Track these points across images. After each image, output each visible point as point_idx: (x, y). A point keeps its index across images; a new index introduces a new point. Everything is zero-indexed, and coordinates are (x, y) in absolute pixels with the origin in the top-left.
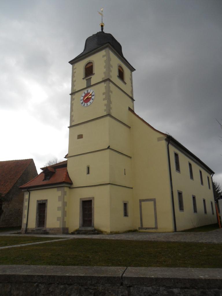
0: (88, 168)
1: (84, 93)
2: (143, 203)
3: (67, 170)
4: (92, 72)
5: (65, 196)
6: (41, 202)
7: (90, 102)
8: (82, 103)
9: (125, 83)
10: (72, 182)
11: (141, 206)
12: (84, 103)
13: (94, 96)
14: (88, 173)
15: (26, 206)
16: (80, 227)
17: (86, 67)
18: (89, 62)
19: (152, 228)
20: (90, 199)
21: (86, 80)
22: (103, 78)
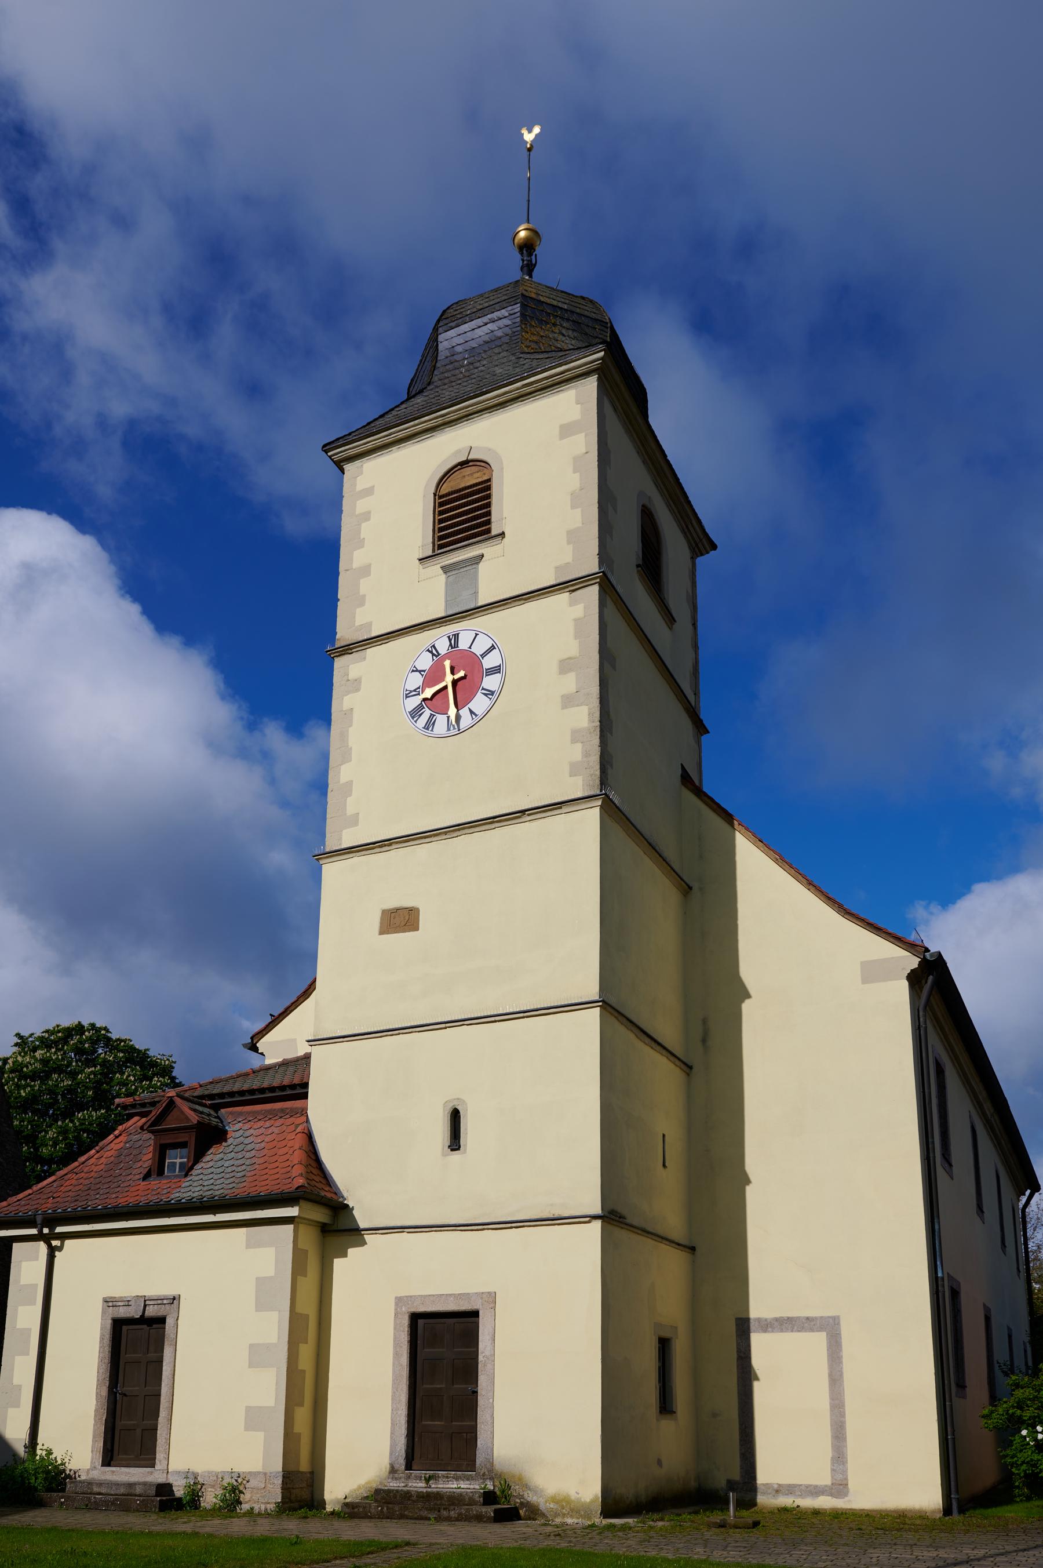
0: (455, 1116)
1: (433, 650)
3: (308, 1121)
4: (489, 522)
5: (300, 1279)
6: (134, 1312)
7: (471, 712)
8: (416, 713)
11: (839, 1457)
12: (427, 712)
16: (393, 1470)
19: (816, 1491)
21: (446, 569)
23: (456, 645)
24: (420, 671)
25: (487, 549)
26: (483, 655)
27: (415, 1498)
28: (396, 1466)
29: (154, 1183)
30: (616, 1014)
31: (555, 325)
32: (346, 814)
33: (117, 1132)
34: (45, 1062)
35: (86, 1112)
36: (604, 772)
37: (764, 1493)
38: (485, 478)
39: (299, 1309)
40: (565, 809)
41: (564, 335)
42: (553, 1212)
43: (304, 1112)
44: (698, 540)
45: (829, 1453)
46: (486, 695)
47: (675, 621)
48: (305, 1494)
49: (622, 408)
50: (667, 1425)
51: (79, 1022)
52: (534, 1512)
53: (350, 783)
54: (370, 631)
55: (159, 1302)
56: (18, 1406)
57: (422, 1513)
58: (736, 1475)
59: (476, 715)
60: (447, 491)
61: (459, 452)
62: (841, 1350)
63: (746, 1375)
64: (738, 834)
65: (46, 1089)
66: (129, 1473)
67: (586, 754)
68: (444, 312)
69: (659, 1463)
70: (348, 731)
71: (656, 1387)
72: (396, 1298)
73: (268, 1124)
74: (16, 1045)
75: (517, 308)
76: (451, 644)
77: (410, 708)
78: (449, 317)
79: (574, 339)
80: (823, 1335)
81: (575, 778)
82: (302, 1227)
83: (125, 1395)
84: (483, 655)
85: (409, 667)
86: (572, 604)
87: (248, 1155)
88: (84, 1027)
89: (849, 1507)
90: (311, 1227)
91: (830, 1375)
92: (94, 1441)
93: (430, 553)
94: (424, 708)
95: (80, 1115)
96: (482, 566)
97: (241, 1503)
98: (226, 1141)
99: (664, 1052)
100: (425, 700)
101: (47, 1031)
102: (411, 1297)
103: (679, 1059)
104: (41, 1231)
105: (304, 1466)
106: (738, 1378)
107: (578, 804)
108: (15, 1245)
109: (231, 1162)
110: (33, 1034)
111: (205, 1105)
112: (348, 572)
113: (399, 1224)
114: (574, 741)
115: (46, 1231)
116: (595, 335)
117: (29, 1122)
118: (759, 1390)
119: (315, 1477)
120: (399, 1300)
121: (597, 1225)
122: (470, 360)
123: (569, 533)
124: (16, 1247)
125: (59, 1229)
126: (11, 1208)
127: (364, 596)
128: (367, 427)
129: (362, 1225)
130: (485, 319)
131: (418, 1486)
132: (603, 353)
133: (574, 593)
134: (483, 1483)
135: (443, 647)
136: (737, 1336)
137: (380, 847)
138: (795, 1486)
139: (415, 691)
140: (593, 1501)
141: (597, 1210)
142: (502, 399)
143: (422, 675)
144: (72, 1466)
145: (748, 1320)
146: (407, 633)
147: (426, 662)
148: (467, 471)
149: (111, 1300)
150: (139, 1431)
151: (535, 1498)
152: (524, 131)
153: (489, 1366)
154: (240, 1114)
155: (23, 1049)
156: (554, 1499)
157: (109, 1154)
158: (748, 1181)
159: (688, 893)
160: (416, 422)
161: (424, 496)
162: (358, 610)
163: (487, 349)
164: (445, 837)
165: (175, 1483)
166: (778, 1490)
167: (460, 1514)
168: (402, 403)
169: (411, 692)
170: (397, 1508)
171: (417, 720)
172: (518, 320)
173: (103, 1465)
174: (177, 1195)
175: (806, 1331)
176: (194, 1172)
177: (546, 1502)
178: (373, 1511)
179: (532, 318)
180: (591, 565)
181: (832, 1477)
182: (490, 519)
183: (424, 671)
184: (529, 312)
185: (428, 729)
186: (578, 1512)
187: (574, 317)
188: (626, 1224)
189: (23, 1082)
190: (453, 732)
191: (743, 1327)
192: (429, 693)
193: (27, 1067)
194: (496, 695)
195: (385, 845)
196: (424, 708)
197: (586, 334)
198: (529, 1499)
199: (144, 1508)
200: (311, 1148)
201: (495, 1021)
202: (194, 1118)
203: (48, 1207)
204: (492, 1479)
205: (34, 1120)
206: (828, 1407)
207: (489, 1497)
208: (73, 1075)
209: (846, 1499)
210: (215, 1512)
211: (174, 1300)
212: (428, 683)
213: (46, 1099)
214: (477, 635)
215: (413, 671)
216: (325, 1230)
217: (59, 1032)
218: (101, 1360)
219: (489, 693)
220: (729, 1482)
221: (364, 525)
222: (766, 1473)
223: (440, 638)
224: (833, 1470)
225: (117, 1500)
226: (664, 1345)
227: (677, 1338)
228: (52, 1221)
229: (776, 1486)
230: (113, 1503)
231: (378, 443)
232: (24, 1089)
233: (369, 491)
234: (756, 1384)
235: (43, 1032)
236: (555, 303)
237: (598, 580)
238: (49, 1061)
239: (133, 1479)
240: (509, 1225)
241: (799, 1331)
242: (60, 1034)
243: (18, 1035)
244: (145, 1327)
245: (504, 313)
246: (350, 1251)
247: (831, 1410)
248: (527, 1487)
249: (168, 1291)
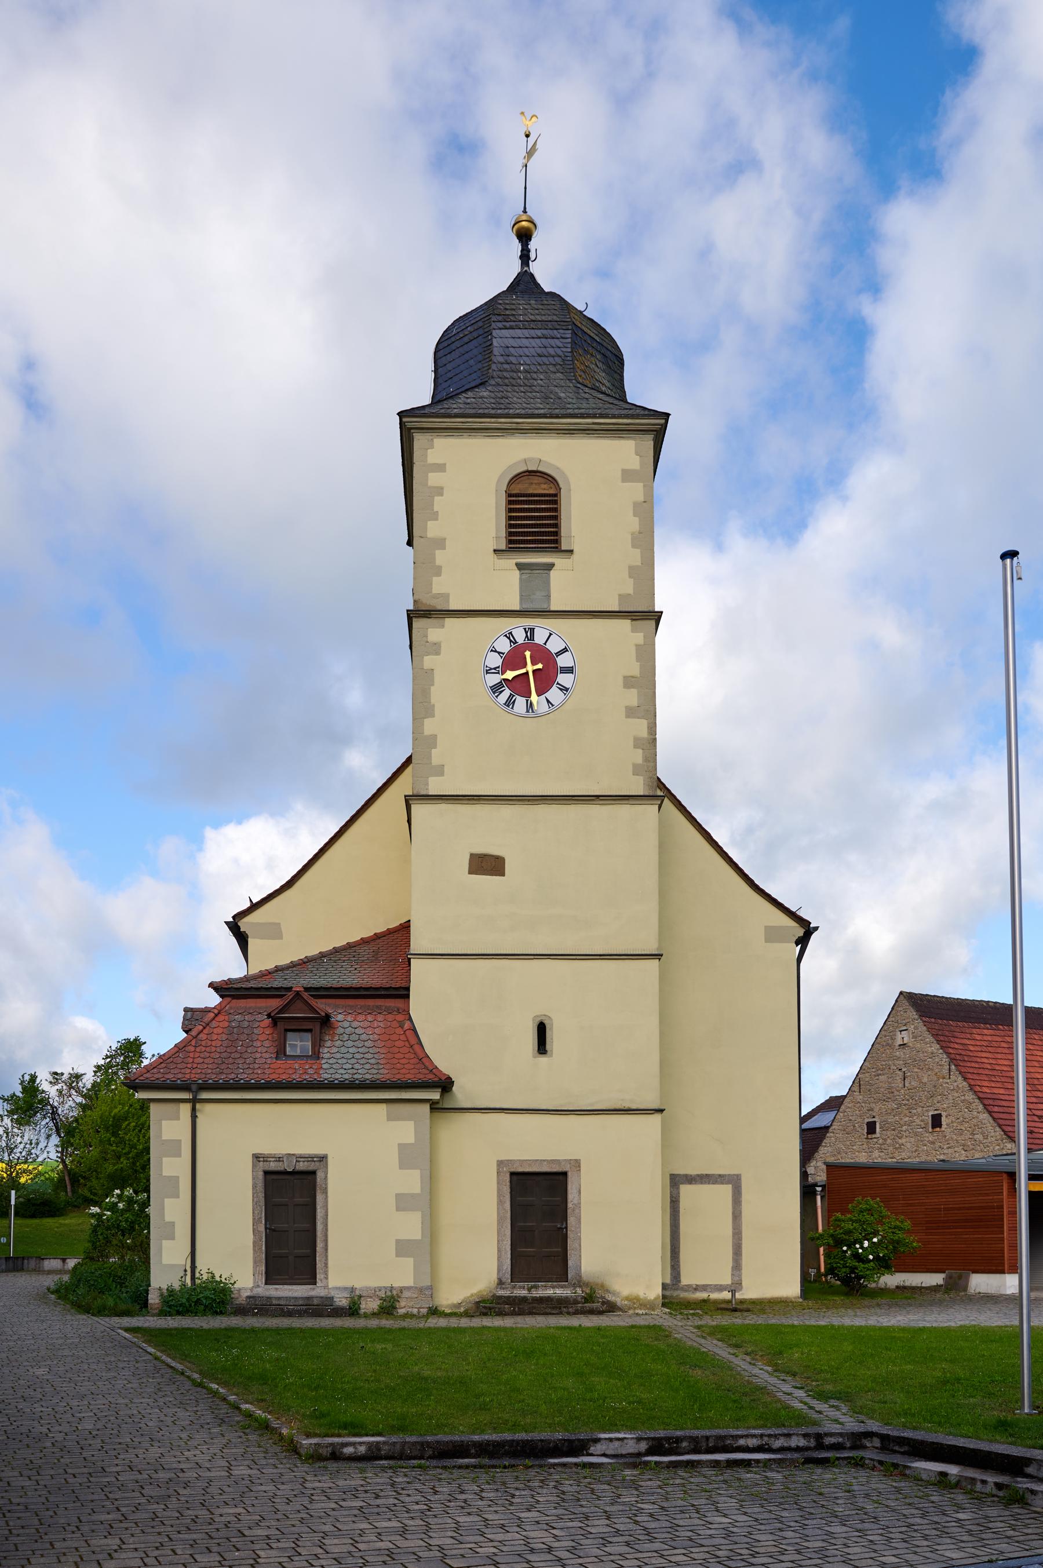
0: (542, 1030)
1: (509, 636)
2: (685, 1190)
8: (496, 689)
11: (737, 1266)
12: (507, 693)
15: (176, 1179)
16: (500, 1283)
18: (532, 467)
19: (720, 1288)
20: (556, 1169)
21: (520, 566)
22: (622, 597)
23: (532, 638)
24: (499, 653)
28: (504, 1280)
32: (431, 763)
42: (624, 1105)
45: (730, 1264)
55: (310, 1159)
57: (547, 1310)
59: (553, 705)
62: (741, 1197)
66: (292, 1290)
70: (430, 689)
72: (498, 1161)
76: (527, 636)
85: (577, 670)
91: (733, 1213)
94: (504, 686)
96: (553, 573)
100: (505, 680)
102: (511, 1160)
107: (642, 800)
112: (422, 539)
114: (636, 746)
120: (500, 1163)
123: (631, 568)
124: (154, 1108)
134: (574, 1289)
135: (520, 637)
136: (671, 1186)
138: (707, 1285)
139: (495, 669)
140: (656, 1299)
143: (502, 657)
147: (504, 646)
148: (536, 480)
149: (262, 1156)
151: (613, 1298)
156: (627, 1298)
161: (496, 491)
164: (527, 803)
171: (498, 695)
177: (622, 1300)
183: (503, 654)
185: (508, 706)
186: (645, 1306)
192: (510, 675)
196: (504, 686)
198: (609, 1299)
199: (467, 1314)
207: (589, 1298)
209: (741, 1292)
214: (551, 634)
215: (492, 651)
218: (255, 1204)
219: (564, 689)
224: (732, 1275)
229: (694, 1286)
233: (441, 468)
239: (296, 1295)
240: (582, 1113)
248: (608, 1291)
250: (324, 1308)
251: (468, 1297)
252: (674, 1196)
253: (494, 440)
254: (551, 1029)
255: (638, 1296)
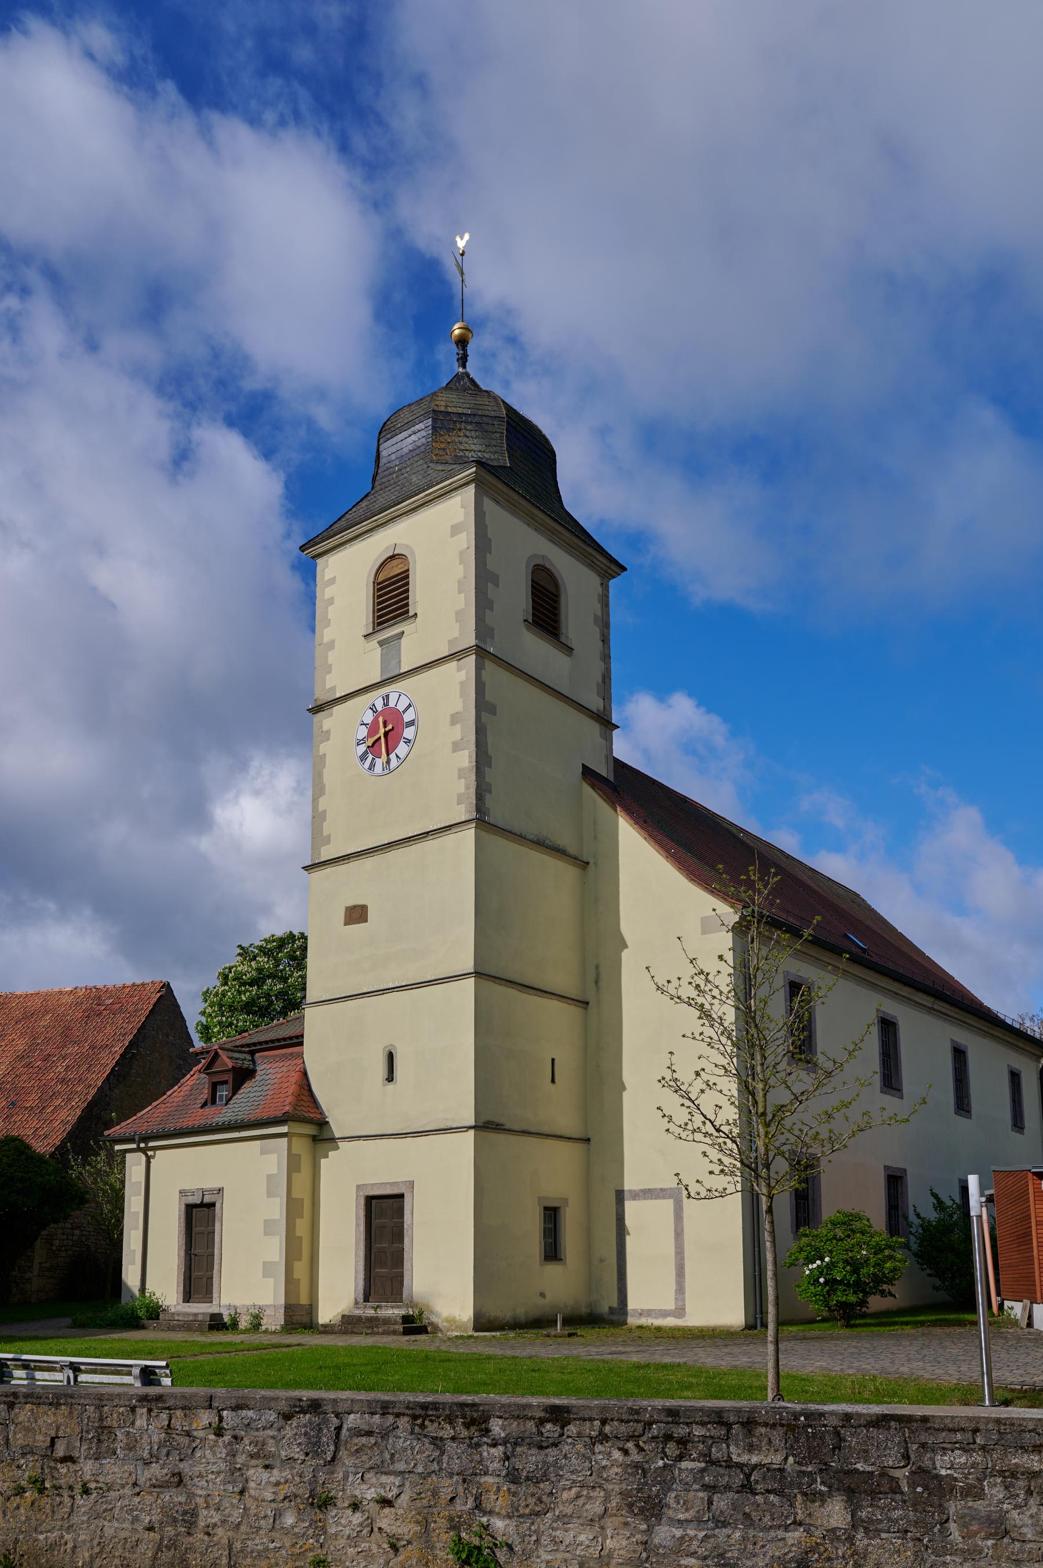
0: (391, 1057)
1: (373, 708)
4: (407, 605)
5: (295, 1175)
7: (397, 756)
8: (363, 758)
9: (568, 650)
10: (322, 1113)
11: (680, 1289)
12: (370, 757)
13: (412, 728)
14: (390, 1078)
16: (356, 1303)
17: (380, 579)
19: (664, 1314)
21: (381, 643)
24: (366, 725)
25: (405, 627)
26: (404, 712)
27: (364, 1320)
28: (358, 1300)
29: (208, 1110)
30: (493, 979)
31: (460, 430)
33: (192, 1073)
34: (260, 970)
35: (296, 1011)
36: (480, 800)
37: (632, 1316)
38: (406, 568)
39: (295, 1194)
40: (454, 830)
41: (468, 437)
43: (301, 1055)
44: (606, 568)
45: (674, 1287)
46: (405, 742)
47: (572, 649)
48: (305, 1320)
49: (504, 498)
50: (553, 1269)
51: (291, 932)
52: (436, 1329)
53: (325, 811)
54: (335, 693)
56: (134, 1264)
58: (615, 1304)
59: (400, 759)
60: (382, 579)
61: (388, 548)
63: (621, 1231)
64: (620, 818)
65: (262, 993)
67: (467, 788)
68: (385, 423)
69: (542, 1295)
71: (540, 1242)
73: (281, 1064)
74: (240, 954)
75: (430, 422)
77: (360, 754)
78: (386, 430)
79: (476, 438)
80: (671, 1201)
81: (461, 806)
82: (295, 1140)
83: (196, 1255)
84: (404, 712)
85: (359, 722)
86: (459, 670)
87: (266, 1088)
88: (295, 936)
89: (686, 1325)
90: (303, 1139)
91: (675, 1230)
92: (178, 1286)
93: (371, 631)
95: (292, 1014)
97: (261, 1325)
98: (255, 1078)
99: (553, 997)
101: (265, 940)
103: (573, 999)
104: (138, 1146)
105: (304, 1300)
106: (617, 1233)
107: (461, 826)
108: (127, 1155)
109: (254, 1094)
110: (252, 944)
111: (244, 1052)
113: (358, 1135)
115: (142, 1145)
116: (494, 430)
117: (251, 1022)
118: (629, 1239)
119: (312, 1309)
121: (472, 1132)
122: (399, 467)
124: (129, 1156)
125: (151, 1144)
126: (122, 1130)
127: (331, 665)
128: (329, 530)
129: (337, 1135)
130: (409, 432)
131: (371, 1312)
132: (475, 468)
133: (460, 661)
135: (379, 706)
137: (343, 860)
138: (652, 1310)
139: (362, 740)
140: (469, 1320)
141: (472, 1123)
142: (413, 506)
144: (166, 1303)
145: (623, 1191)
146: (357, 694)
147: (369, 717)
148: (394, 562)
150: (205, 1279)
151: (436, 1319)
152: (458, 239)
153: (410, 1231)
154: (266, 1057)
155: (245, 959)
156: (447, 1320)
157: (186, 1088)
158: (624, 1089)
159: (586, 867)
160: (359, 526)
162: (328, 676)
163: (410, 457)
164: (381, 852)
165: (224, 1313)
166: (641, 1314)
167: (384, 1330)
168: (354, 507)
169: (360, 741)
170: (349, 1327)
172: (430, 432)
173: (184, 1302)
174: (217, 1119)
175: (660, 1199)
176: (232, 1102)
178: (336, 1329)
179: (441, 428)
180: (471, 640)
181: (676, 1303)
182: (408, 603)
183: (368, 724)
184: (439, 424)
186: (460, 1328)
187: (477, 419)
188: (505, 1130)
189: (243, 988)
190: (386, 772)
191: (620, 1197)
193: (246, 975)
194: (412, 742)
195: (346, 859)
197: (486, 431)
199: (200, 1329)
200: (305, 1081)
201: (412, 989)
202: (230, 1064)
203: (144, 1129)
204: (412, 1307)
205: (255, 1021)
206: (674, 1254)
207: (406, 1319)
208: (285, 980)
209: (684, 1319)
210: (246, 1331)
211: (220, 1190)
212: (370, 734)
213: (263, 1001)
216: (315, 1139)
217: (274, 941)
220: (610, 1308)
221: (329, 608)
222: (633, 1303)
223: (376, 698)
224: (676, 1299)
225: (185, 1324)
226: (552, 1215)
227: (568, 1206)
228: (146, 1139)
229: (640, 1311)
230: (183, 1326)
231: (336, 543)
232: (245, 994)
233: (333, 581)
234: (627, 1237)
235: (261, 941)
236: (460, 411)
237: (474, 651)
238: (262, 970)
241: (656, 1199)
242: (275, 944)
243: (239, 946)
244: (206, 1209)
245: (421, 426)
246: (330, 1153)
247: (676, 1256)
248: (432, 1312)
249: (217, 1185)
250: (216, 1323)
251: (336, 1316)
252: (620, 1213)
253: (370, 540)
254: (396, 1057)
255: (455, 1317)
